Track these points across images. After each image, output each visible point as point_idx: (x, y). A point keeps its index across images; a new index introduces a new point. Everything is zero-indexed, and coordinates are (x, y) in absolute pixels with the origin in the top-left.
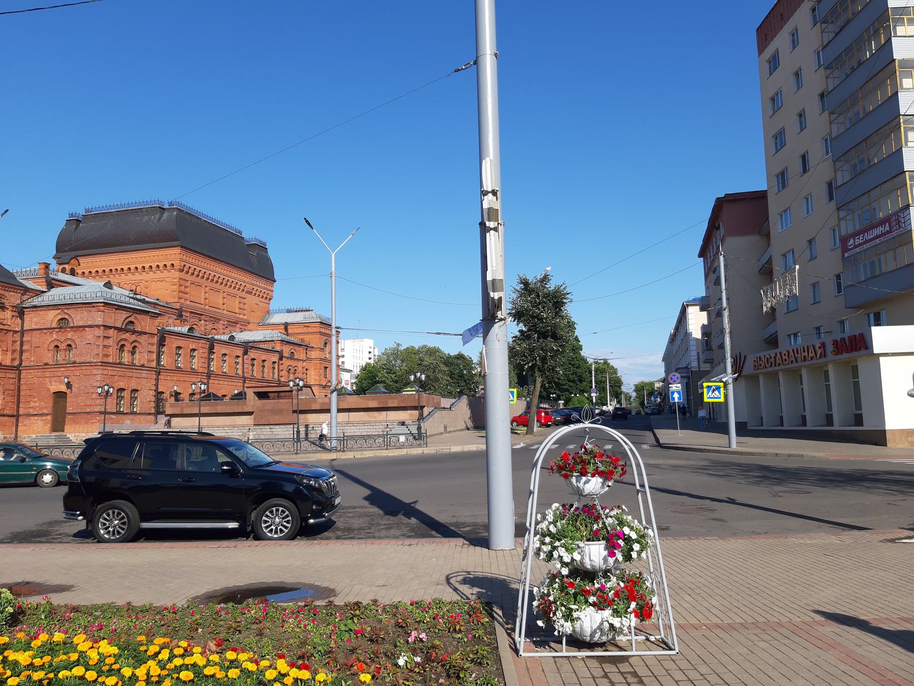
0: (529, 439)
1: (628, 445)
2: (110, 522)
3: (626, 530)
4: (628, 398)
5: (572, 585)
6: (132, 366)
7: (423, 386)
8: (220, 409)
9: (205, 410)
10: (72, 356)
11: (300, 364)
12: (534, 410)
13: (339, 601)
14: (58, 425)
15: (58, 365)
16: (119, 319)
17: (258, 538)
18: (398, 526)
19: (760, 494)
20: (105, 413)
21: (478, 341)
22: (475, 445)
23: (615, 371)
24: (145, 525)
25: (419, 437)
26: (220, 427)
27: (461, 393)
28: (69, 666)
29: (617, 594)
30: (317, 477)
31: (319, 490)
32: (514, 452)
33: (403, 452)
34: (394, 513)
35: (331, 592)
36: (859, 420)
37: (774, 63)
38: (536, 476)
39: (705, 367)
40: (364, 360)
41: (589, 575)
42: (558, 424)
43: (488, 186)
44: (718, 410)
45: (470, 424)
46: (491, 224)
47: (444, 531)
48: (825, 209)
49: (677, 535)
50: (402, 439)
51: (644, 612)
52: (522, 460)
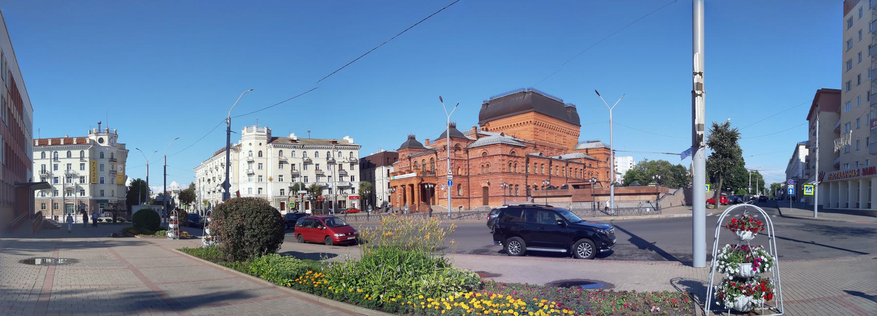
0: (715, 211)
1: (765, 215)
2: (513, 247)
3: (762, 258)
4: (767, 191)
5: (734, 285)
6: (515, 173)
7: (660, 182)
8: (556, 194)
9: (549, 194)
10: (489, 170)
11: (594, 170)
12: (718, 196)
13: (616, 290)
14: (486, 203)
15: (484, 174)
16: (508, 151)
17: (576, 257)
18: (646, 254)
19: (826, 240)
20: (505, 196)
21: (690, 158)
22: (686, 214)
23: (761, 177)
24: (528, 249)
25: (657, 209)
26: (557, 203)
27: (680, 186)
28: (508, 309)
29: (756, 288)
30: (604, 229)
31: (605, 235)
32: (707, 218)
33: (649, 217)
34: (644, 248)
35: (612, 286)
36: (869, 206)
37: (850, 23)
38: (718, 230)
39: (806, 177)
40: (628, 168)
41: (743, 280)
42: (731, 204)
43: (697, 70)
44: (810, 198)
45: (684, 203)
46: (698, 92)
47: (670, 258)
48: (865, 104)
49: (787, 259)
50: (648, 210)
51: (769, 297)
52: (711, 222)
